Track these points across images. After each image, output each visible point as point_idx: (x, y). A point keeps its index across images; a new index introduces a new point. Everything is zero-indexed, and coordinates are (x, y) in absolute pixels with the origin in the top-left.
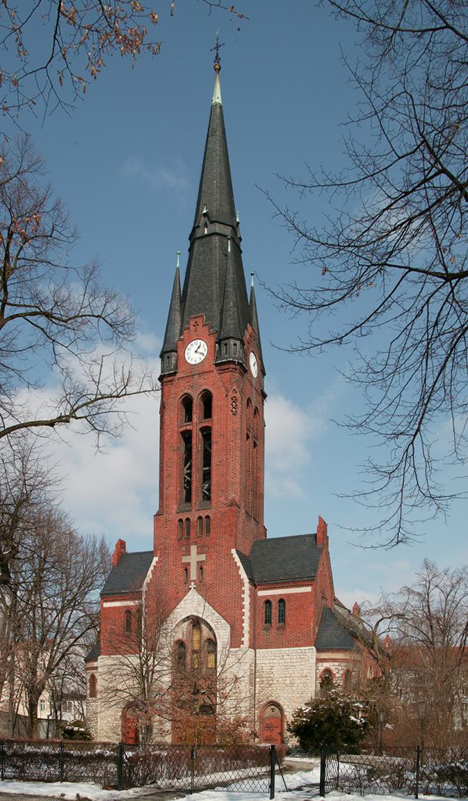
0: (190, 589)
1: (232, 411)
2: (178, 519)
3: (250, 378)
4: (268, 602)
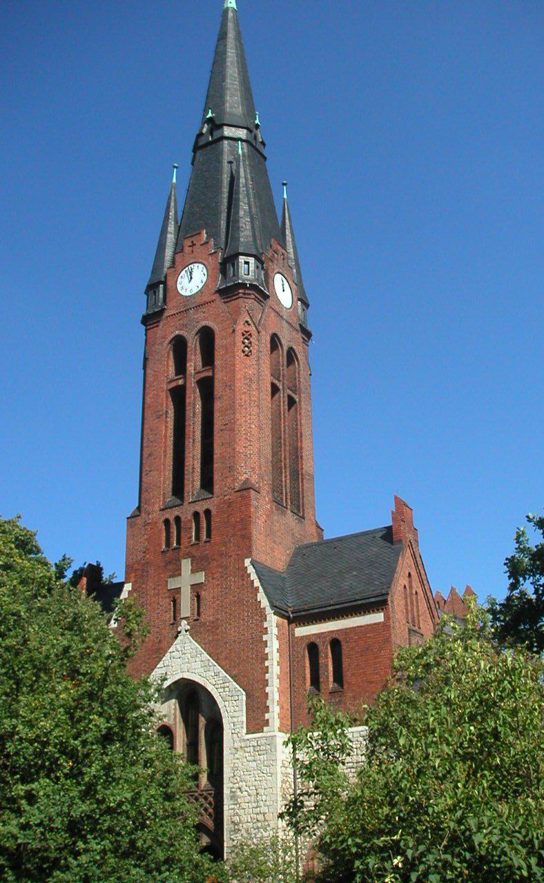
0: (180, 632)
1: (243, 352)
2: (163, 519)
3: (276, 307)
4: (313, 648)
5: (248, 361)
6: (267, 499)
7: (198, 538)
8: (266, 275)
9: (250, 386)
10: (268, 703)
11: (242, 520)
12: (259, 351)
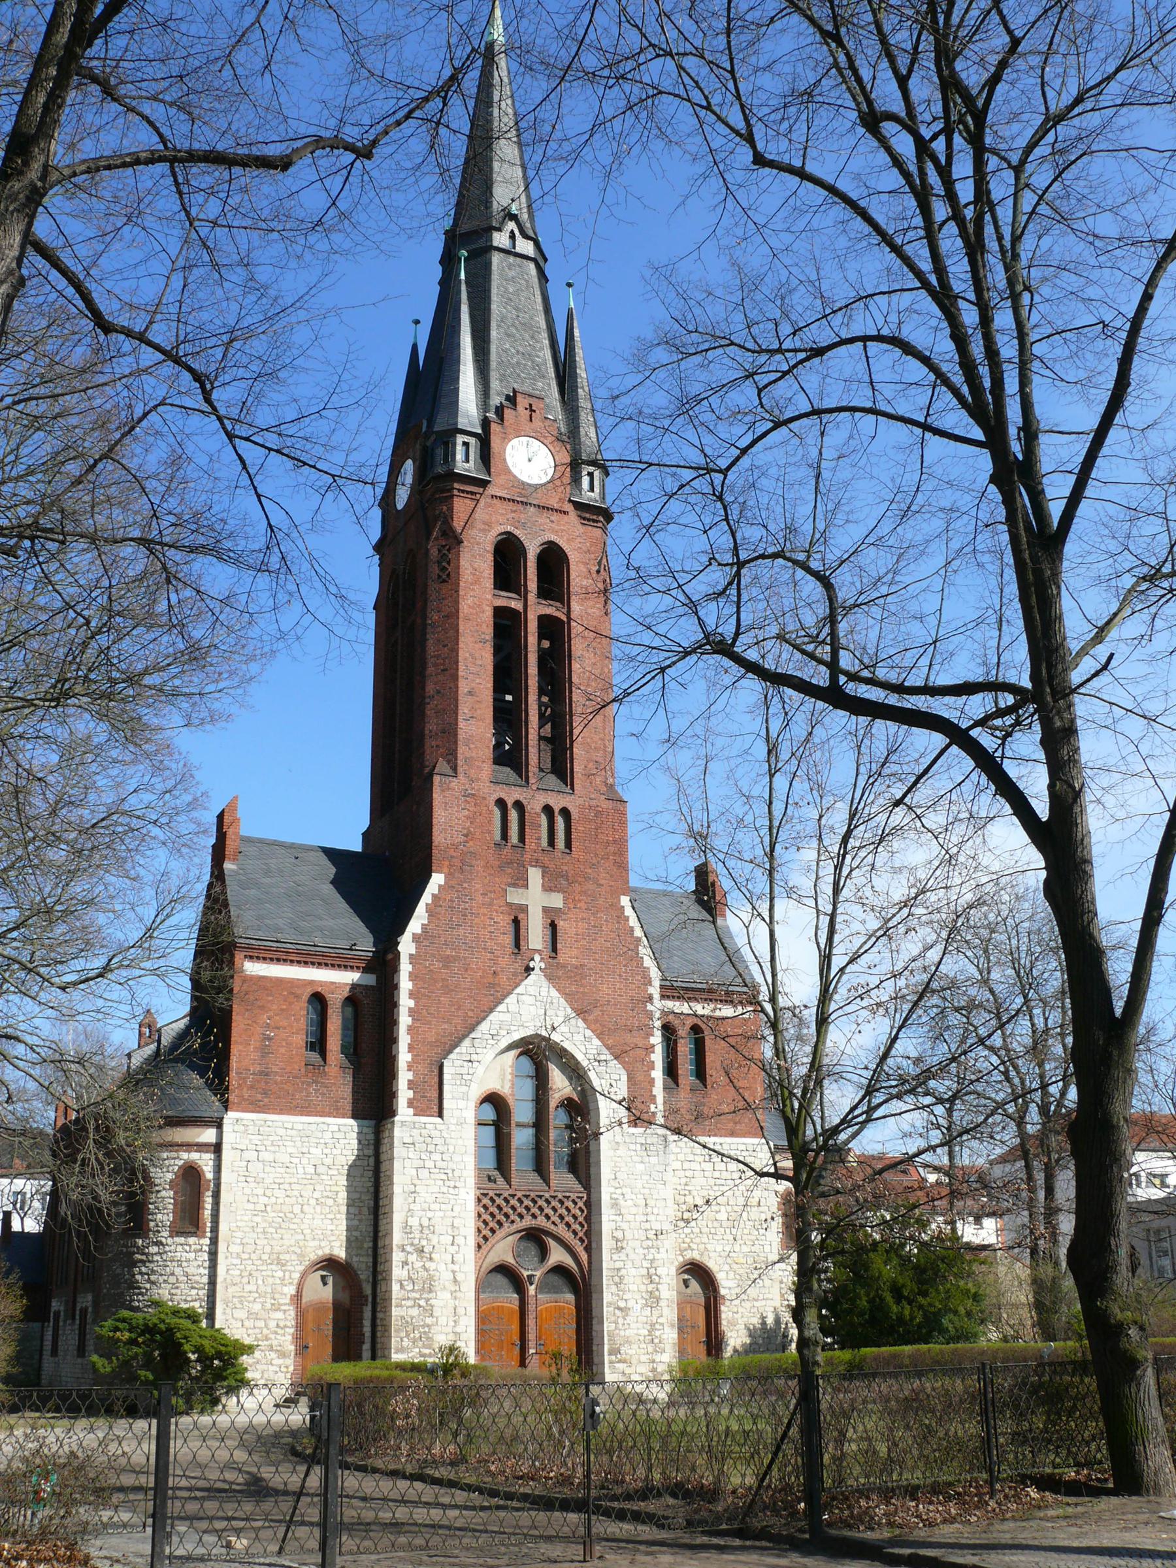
2: (496, 796)
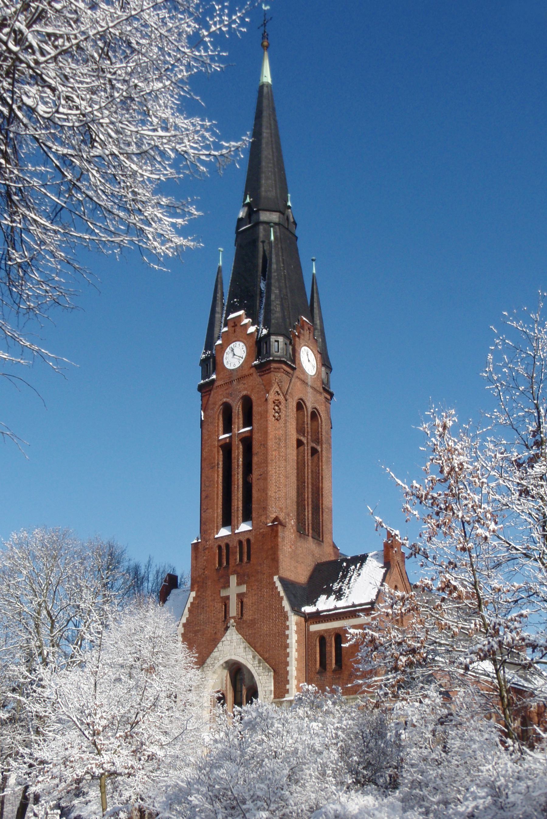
1: (274, 416)
3: (302, 376)
4: (322, 639)
5: (278, 424)
6: (292, 531)
7: (241, 559)
8: (294, 350)
9: (279, 444)
10: (289, 678)
11: (272, 548)
12: (286, 416)
